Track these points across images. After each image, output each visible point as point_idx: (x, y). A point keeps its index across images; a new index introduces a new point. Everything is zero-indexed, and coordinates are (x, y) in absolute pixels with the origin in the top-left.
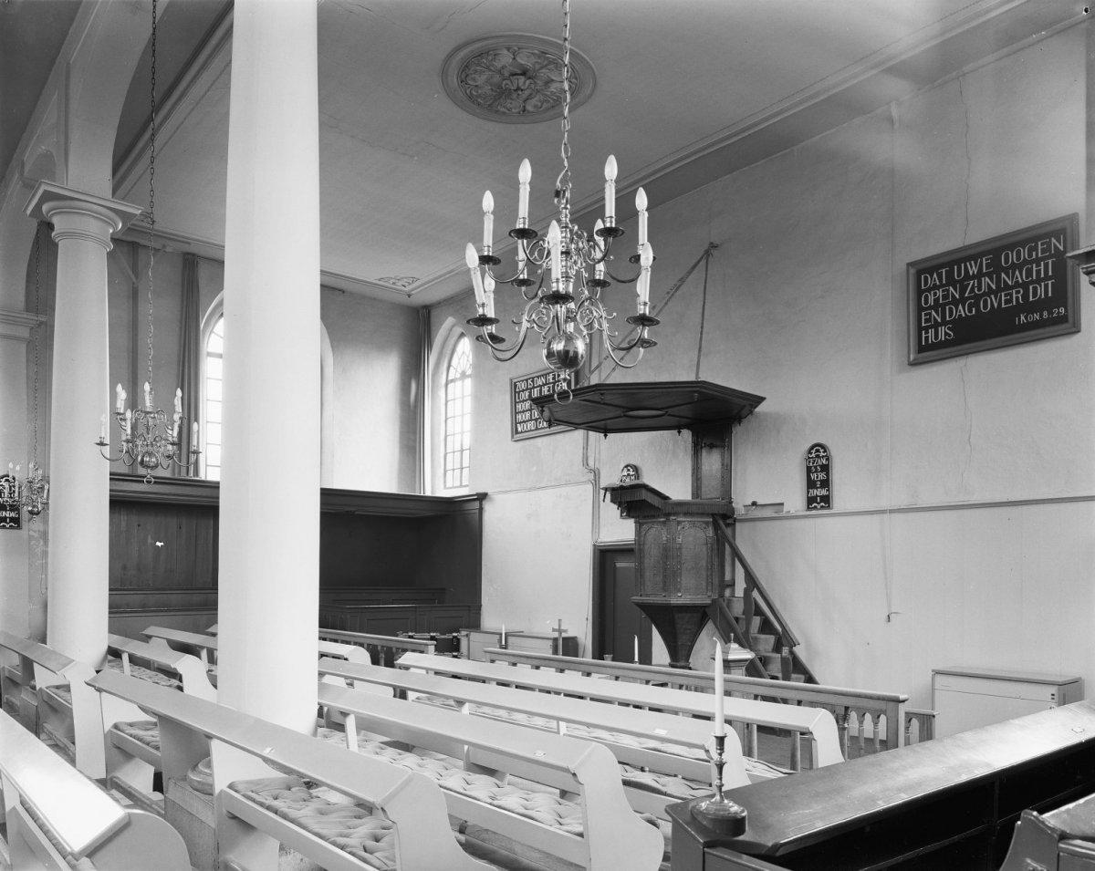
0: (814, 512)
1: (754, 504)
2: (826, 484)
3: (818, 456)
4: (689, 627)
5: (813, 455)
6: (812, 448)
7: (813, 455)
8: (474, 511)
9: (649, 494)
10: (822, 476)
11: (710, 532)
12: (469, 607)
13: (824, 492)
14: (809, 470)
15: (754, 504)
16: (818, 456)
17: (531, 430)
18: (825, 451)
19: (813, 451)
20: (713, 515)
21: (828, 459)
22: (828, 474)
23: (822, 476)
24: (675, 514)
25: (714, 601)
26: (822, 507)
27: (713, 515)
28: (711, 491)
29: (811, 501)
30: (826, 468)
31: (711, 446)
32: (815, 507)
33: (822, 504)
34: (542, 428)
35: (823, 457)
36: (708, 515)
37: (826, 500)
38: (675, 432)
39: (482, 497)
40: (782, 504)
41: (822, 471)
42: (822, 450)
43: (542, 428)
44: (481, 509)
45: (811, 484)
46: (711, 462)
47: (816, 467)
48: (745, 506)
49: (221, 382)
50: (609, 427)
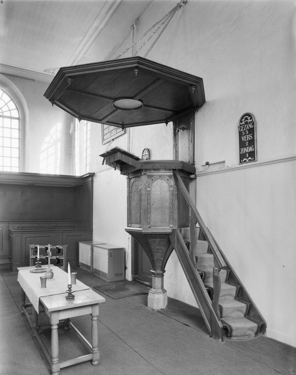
0: (244, 165)
1: (207, 164)
2: (252, 142)
3: (246, 123)
4: (160, 248)
5: (243, 123)
6: (242, 118)
7: (243, 123)
8: (89, 182)
9: (124, 156)
10: (249, 137)
11: (172, 182)
12: (86, 230)
13: (251, 149)
14: (241, 134)
15: (207, 164)
16: (246, 123)
17: (109, 138)
18: (251, 118)
19: (244, 120)
20: (174, 170)
21: (253, 124)
22: (253, 136)
23: (249, 137)
24: (146, 170)
25: (173, 230)
26: (250, 160)
27: (174, 170)
28: (184, 157)
29: (242, 157)
30: (252, 131)
31: (183, 129)
32: (245, 161)
33: (250, 158)
34: (113, 136)
35: (250, 122)
36: (170, 170)
37: (252, 155)
38: (164, 124)
39: (92, 175)
40: (224, 162)
41: (249, 134)
42: (249, 118)
43: (113, 136)
44: (92, 181)
45: (242, 145)
46: (184, 138)
47: (245, 131)
48: (202, 166)
49: (234, 335)
50: (125, 123)
